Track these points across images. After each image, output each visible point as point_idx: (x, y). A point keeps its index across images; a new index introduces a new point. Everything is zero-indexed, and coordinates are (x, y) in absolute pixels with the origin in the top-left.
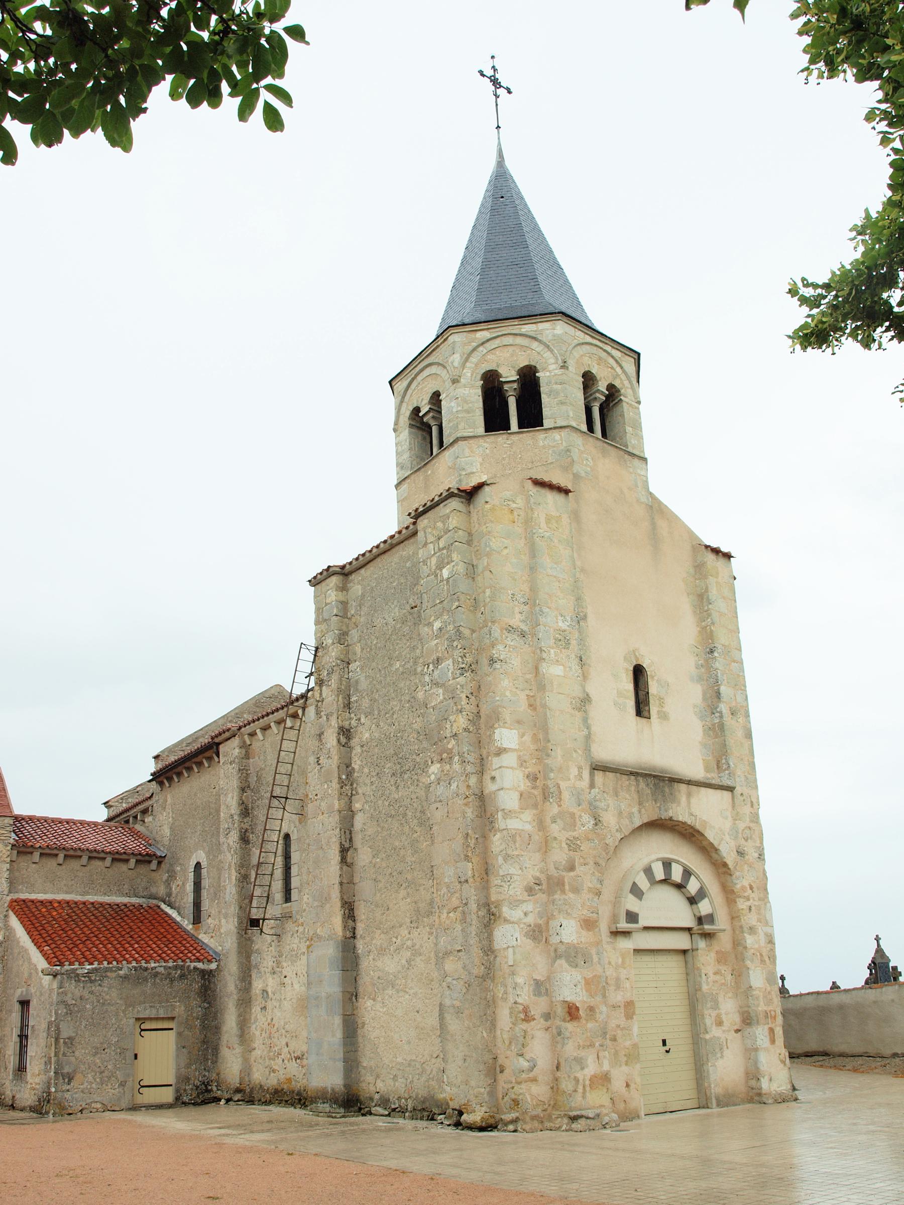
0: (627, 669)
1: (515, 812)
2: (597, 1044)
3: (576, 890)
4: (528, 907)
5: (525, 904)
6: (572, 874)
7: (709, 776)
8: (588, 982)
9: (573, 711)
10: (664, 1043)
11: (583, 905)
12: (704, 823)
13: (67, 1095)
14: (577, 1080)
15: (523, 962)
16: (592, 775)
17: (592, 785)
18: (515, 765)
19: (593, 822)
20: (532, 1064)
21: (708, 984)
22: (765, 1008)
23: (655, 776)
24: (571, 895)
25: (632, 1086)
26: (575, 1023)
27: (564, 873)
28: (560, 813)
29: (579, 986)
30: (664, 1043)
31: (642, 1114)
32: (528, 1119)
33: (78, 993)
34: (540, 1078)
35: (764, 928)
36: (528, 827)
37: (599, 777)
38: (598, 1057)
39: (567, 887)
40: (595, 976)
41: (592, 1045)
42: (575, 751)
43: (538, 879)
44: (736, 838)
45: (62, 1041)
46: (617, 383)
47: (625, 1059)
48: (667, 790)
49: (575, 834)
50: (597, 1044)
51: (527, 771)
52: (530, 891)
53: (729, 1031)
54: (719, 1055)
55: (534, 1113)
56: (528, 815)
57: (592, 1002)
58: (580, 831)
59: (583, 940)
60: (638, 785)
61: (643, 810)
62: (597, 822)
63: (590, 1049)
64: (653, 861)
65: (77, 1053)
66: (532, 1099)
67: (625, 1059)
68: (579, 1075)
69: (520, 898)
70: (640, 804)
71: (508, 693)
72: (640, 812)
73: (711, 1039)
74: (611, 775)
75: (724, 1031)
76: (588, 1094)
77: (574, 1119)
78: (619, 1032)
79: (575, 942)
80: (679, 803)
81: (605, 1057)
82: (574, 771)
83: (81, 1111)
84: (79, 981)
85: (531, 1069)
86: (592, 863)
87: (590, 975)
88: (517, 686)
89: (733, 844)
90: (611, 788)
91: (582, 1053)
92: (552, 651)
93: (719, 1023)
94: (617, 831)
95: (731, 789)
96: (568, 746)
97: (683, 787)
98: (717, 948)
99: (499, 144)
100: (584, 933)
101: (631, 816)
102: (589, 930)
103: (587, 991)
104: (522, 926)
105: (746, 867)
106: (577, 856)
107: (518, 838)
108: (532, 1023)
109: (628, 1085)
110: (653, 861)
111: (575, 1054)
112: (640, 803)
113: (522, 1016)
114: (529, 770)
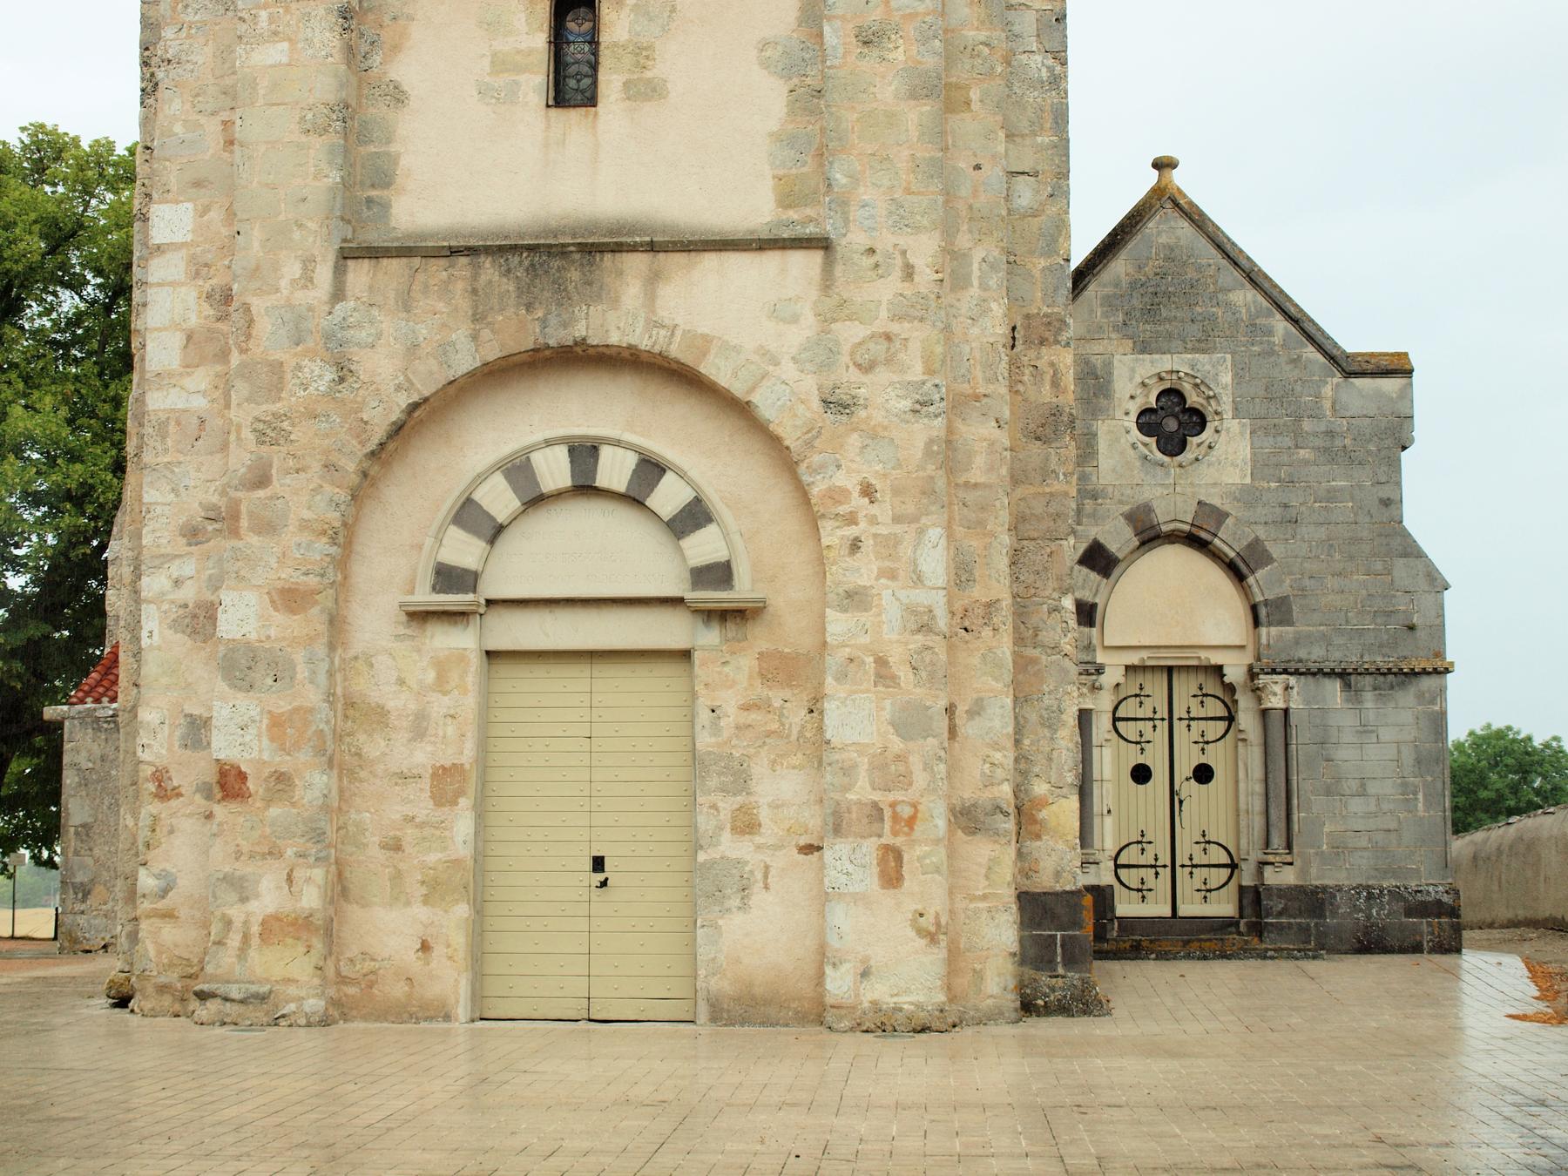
1: (171, 375)
2: (290, 852)
3: (268, 527)
4: (188, 568)
5: (177, 562)
6: (261, 493)
7: (793, 215)
8: (277, 724)
9: (304, 138)
10: (598, 864)
11: (282, 558)
12: (705, 343)
13: (81, 920)
14: (228, 923)
15: (164, 680)
16: (339, 272)
17: (338, 294)
18: (182, 277)
19: (330, 375)
20: (162, 883)
21: (715, 728)
22: (876, 796)
23: (531, 248)
24: (254, 540)
25: (439, 950)
26: (234, 806)
27: (240, 494)
28: (243, 365)
29: (253, 730)
30: (598, 864)
32: (150, 990)
33: (96, 750)
34: (183, 913)
35: (902, 594)
36: (199, 403)
37: (360, 274)
38: (290, 879)
39: (244, 523)
40: (296, 710)
41: (274, 853)
42: (300, 226)
43: (215, 508)
44: (825, 366)
45: (72, 830)
47: (424, 890)
49: (278, 407)
50: (290, 852)
51: (207, 287)
52: (193, 534)
53: (778, 847)
55: (163, 979)
56: (201, 379)
57: (284, 763)
58: (293, 398)
59: (273, 632)
61: (486, 334)
63: (270, 860)
65: (96, 851)
66: (159, 953)
67: (424, 890)
68: (236, 913)
69: (169, 550)
71: (178, 128)
72: (475, 337)
73: (714, 862)
74: (394, 265)
75: (758, 847)
76: (253, 953)
77: (203, 996)
79: (253, 636)
80: (615, 302)
81: (308, 880)
82: (293, 269)
83: (105, 947)
84: (99, 729)
85: (164, 893)
86: (316, 467)
87: (284, 706)
88: (200, 107)
89: (809, 385)
90: (392, 295)
91: (245, 868)
92: (264, 14)
93: (746, 825)
94: (398, 388)
95: (822, 244)
96: (282, 217)
97: (636, 263)
98: (763, 645)
100: (279, 618)
101: (445, 350)
102: (293, 612)
103: (272, 740)
104: (165, 607)
106: (277, 457)
107: (172, 428)
108: (174, 803)
109: (425, 947)
111: (227, 869)
112: (477, 317)
113: (152, 787)
114: (214, 281)
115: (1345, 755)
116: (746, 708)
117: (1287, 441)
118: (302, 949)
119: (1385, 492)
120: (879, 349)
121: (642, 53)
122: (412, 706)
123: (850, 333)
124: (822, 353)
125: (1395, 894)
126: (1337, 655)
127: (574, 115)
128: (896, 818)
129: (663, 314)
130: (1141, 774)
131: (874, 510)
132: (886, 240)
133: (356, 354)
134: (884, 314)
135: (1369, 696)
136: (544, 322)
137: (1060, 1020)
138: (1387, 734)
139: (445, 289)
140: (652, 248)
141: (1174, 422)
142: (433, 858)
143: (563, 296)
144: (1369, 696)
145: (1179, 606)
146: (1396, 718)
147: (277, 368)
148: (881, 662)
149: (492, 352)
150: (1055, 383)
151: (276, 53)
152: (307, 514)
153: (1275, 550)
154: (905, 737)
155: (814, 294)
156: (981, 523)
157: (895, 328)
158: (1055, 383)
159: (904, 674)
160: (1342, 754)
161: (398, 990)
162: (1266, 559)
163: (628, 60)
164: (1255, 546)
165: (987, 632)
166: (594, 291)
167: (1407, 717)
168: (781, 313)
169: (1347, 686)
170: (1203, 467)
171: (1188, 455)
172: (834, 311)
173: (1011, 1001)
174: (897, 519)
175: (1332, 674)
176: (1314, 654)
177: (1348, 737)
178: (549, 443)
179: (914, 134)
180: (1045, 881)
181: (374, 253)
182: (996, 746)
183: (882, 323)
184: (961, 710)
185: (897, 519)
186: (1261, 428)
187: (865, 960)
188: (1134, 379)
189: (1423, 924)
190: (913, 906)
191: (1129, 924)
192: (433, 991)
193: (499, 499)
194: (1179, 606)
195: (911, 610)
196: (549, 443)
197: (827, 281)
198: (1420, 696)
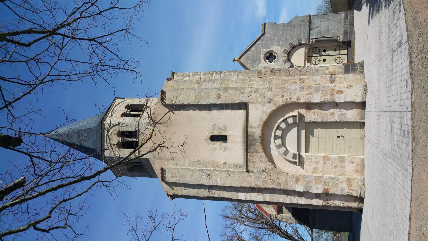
0: (213, 144)
2: (337, 182)
10: (339, 137)
17: (253, 172)
19: (264, 173)
23: (247, 144)
30: (339, 137)
31: (362, 156)
37: (250, 169)
38: (341, 182)
41: (337, 185)
46: (120, 116)
48: (251, 138)
49: (269, 181)
50: (337, 182)
54: (345, 116)
57: (323, 182)
60: (251, 152)
61: (259, 151)
62: (264, 171)
64: (275, 144)
70: (257, 152)
72: (259, 152)
78: (333, 164)
80: (255, 132)
82: (249, 178)
87: (314, 182)
89: (267, 105)
97: (249, 130)
99: (74, 197)
100: (300, 182)
105: (275, 99)
106: (276, 181)
109: (352, 163)
110: (275, 144)
112: (256, 152)
115: (322, 29)
116: (314, 114)
117: (274, 41)
118: (352, 181)
119: (282, 26)
120: (262, 95)
121: (220, 129)
122: (314, 163)
123: (260, 99)
124: (263, 104)
125: (344, 21)
126: (307, 32)
127: (228, 138)
128: (332, 92)
129: (257, 126)
130: (324, 60)
131: (285, 96)
132: (247, 95)
133: (261, 170)
134: (257, 95)
135: (313, 26)
136: (257, 143)
137: (364, 67)
138: (319, 24)
139: (252, 157)
140: (247, 127)
141: (270, 57)
142: (338, 161)
143: (254, 140)
144: (313, 26)
145: (299, 57)
146: (316, 22)
147: (263, 181)
148: (308, 94)
149: (262, 150)
150: (267, 71)
151: (219, 180)
152: (285, 178)
153: (290, 42)
154: (320, 91)
155: (254, 105)
156: (287, 81)
157: (259, 93)
158: (267, 71)
159: (310, 91)
160: (322, 30)
161: (359, 167)
162: (292, 43)
163: (221, 131)
164: (290, 44)
165: (304, 80)
166: (253, 136)
167: (316, 20)
168: (257, 109)
169: (312, 30)
170: (278, 53)
171: (276, 55)
172: (256, 102)
173: (362, 74)
174: (287, 93)
175: (310, 32)
176: (307, 35)
177: (319, 29)
178: (275, 142)
179: (232, 91)
180: (342, 70)
181: (247, 167)
182: (321, 78)
183: (258, 95)
184: (315, 83)
185: (287, 93)
186: (272, 45)
187: (355, 96)
188: (264, 64)
189: (349, 16)
190: (346, 89)
191: (349, 61)
192: (359, 162)
193: (283, 150)
194: (299, 57)
195: (300, 90)
196: (275, 142)
197: (253, 103)
198: (313, 19)
